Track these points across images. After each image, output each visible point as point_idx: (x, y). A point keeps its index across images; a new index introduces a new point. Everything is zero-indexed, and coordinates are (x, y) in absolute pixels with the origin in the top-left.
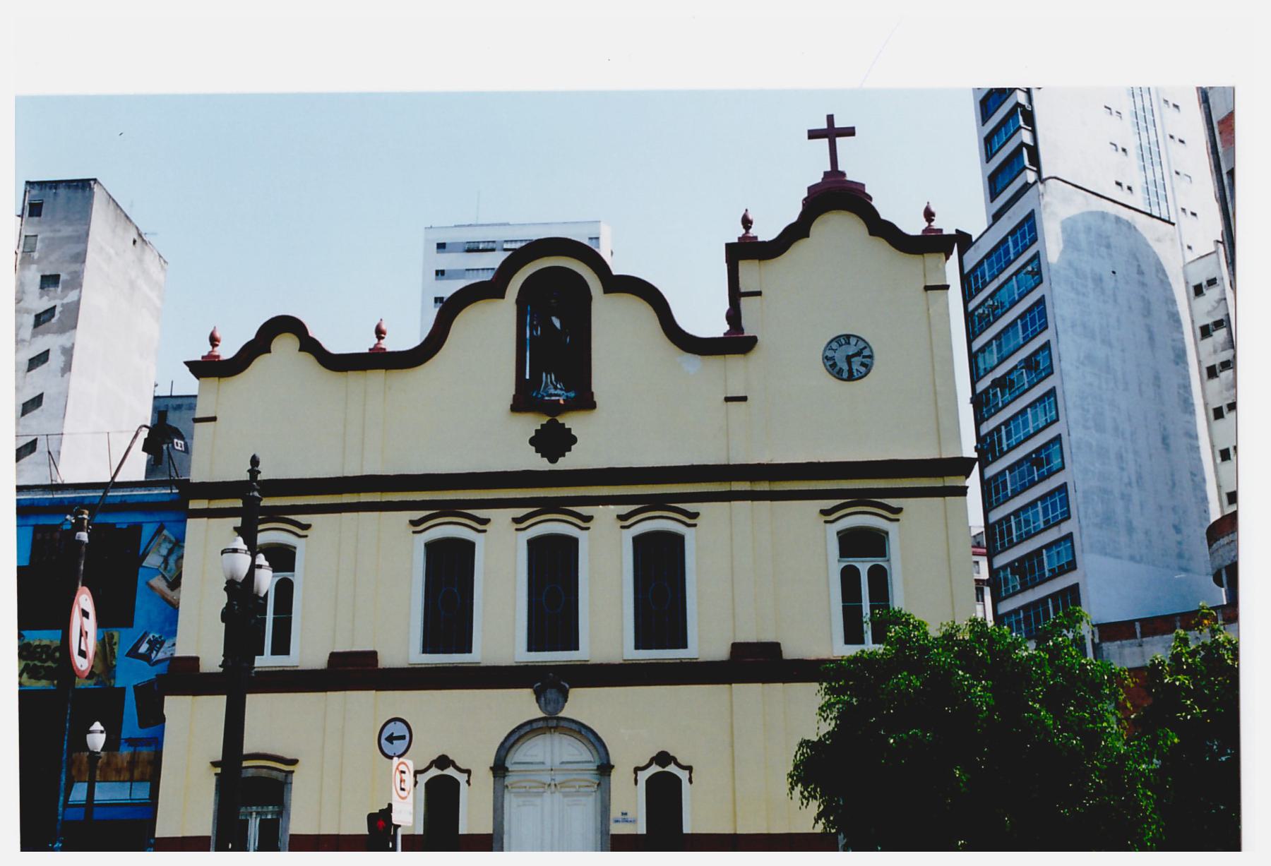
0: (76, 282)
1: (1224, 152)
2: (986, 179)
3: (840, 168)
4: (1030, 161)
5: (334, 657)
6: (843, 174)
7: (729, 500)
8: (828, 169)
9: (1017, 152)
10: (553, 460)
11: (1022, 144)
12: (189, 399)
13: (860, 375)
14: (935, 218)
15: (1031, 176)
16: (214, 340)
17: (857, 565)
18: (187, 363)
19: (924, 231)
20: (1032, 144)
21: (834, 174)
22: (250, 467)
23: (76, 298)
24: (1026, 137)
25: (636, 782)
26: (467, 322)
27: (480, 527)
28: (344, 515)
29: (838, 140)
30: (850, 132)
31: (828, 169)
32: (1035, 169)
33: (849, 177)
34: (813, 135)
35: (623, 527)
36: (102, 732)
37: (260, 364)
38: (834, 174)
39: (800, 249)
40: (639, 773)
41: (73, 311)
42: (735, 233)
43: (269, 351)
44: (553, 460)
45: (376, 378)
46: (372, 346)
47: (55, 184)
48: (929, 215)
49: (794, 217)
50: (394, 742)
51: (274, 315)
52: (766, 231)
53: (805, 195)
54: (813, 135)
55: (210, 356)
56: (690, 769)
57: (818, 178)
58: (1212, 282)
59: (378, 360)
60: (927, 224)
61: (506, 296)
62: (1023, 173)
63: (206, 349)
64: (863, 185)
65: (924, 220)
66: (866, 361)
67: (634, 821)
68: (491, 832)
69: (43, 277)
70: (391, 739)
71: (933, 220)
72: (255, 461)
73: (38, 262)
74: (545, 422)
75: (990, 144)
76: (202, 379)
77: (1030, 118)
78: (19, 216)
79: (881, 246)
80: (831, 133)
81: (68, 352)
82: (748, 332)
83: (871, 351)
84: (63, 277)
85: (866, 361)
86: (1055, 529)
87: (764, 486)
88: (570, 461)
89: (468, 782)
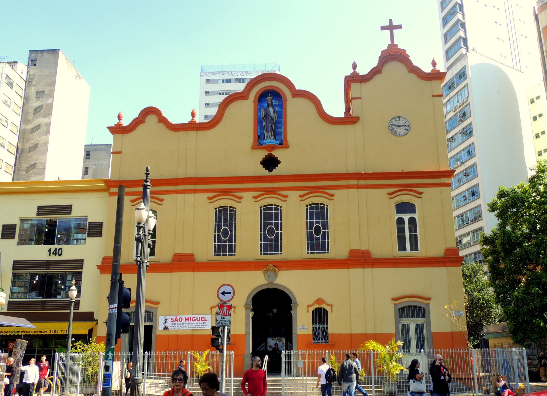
0: (51, 95)
1: (544, 42)
2: (445, 52)
3: (395, 43)
4: (463, 45)
5: (351, 252)
6: (396, 46)
7: (348, 188)
8: (390, 43)
9: (458, 40)
10: (270, 171)
11: (461, 37)
12: (96, 146)
13: (405, 134)
14: (437, 65)
15: (464, 51)
16: (119, 117)
18: (107, 127)
19: (432, 71)
20: (464, 37)
21: (392, 46)
23: (51, 102)
24: (462, 35)
25: (308, 311)
26: (234, 108)
28: (350, 190)
29: (394, 31)
30: (399, 27)
31: (390, 43)
32: (466, 48)
33: (399, 47)
34: (383, 28)
35: (301, 200)
36: (75, 290)
37: (141, 128)
38: (392, 46)
39: (378, 78)
41: (50, 107)
42: (349, 72)
44: (270, 171)
45: (192, 134)
46: (190, 121)
47: (42, 51)
48: (354, 66)
50: (225, 295)
51: (149, 106)
52: (363, 70)
53: (380, 55)
54: (383, 28)
55: (118, 124)
56: (331, 306)
57: (385, 48)
58: (538, 98)
59: (192, 126)
60: (433, 68)
61: (249, 98)
62: (461, 49)
63: (116, 121)
64: (405, 51)
65: (432, 66)
66: (407, 128)
68: (244, 332)
70: (223, 293)
71: (436, 66)
73: (35, 86)
75: (446, 37)
76: (115, 135)
77: (463, 25)
78: (27, 65)
79: (413, 76)
80: (391, 27)
81: (48, 125)
82: (354, 115)
83: (409, 123)
84: (46, 92)
85: (407, 128)
86: (473, 203)
87: (362, 182)
89: (332, 310)
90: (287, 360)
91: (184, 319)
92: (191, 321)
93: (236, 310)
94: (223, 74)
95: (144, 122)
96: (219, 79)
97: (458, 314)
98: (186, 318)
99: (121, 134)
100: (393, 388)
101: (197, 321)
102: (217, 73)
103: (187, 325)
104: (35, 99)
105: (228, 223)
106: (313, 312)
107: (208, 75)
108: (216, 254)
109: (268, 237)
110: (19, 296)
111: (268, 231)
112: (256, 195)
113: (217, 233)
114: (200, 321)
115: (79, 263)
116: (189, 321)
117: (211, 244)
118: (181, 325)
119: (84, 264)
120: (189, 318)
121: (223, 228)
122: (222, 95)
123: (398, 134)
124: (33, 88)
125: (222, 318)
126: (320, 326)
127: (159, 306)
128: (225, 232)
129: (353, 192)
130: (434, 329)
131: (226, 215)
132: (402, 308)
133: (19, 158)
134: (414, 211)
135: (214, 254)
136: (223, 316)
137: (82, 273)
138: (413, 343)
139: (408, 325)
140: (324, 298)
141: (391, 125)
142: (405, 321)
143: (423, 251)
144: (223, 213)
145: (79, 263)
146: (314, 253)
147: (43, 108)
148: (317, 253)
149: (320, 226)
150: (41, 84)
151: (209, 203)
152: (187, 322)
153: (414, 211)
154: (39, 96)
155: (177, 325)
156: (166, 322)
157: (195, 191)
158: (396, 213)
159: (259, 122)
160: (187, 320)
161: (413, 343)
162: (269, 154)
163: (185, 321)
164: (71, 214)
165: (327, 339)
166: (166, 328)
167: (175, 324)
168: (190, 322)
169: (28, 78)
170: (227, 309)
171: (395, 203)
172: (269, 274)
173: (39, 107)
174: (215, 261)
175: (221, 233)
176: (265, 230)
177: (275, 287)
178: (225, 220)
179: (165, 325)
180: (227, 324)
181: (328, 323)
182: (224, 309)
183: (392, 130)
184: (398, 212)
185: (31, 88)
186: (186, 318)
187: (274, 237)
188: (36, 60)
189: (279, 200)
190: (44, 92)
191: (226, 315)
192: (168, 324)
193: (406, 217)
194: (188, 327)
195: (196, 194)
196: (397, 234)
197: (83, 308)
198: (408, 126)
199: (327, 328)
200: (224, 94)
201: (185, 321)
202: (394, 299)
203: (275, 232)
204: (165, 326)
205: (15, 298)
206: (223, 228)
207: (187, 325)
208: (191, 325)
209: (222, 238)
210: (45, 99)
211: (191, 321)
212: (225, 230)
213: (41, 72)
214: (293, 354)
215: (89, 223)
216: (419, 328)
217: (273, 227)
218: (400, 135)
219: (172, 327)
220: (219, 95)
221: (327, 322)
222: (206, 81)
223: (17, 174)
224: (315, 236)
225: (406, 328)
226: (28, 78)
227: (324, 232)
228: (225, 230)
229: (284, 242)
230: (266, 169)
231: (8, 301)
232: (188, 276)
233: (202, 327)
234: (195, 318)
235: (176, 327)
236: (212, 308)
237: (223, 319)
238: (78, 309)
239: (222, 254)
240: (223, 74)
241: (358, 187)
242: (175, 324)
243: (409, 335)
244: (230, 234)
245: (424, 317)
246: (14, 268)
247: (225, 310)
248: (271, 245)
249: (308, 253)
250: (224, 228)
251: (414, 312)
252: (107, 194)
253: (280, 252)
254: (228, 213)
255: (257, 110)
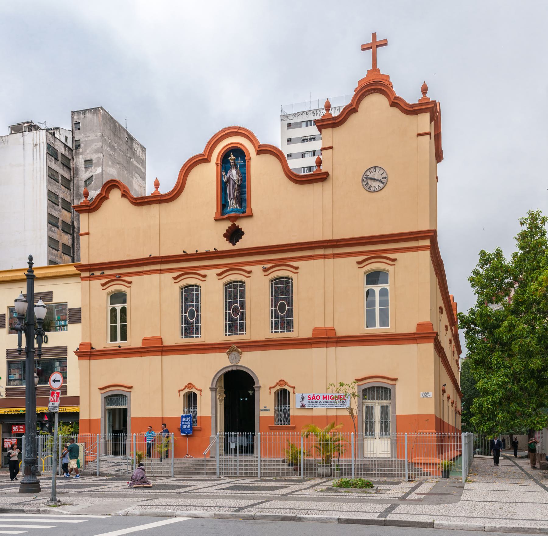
10: (234, 244)
13: (380, 189)
17: (373, 288)
22: (28, 261)
25: (180, 395)
27: (203, 279)
28: (316, 261)
30: (384, 43)
34: (365, 48)
39: (354, 119)
40: (180, 392)
43: (441, 162)
44: (234, 244)
45: (154, 209)
47: (84, 111)
48: (424, 90)
49: (348, 102)
54: (365, 48)
56: (294, 388)
67: (269, 410)
68: (210, 415)
69: (85, 161)
72: (31, 258)
74: (230, 226)
79: (396, 111)
83: (387, 174)
84: (94, 161)
87: (330, 251)
88: (243, 244)
89: (201, 394)
90: (226, 442)
91: (321, 397)
92: (329, 399)
93: (295, 390)
94: (307, 114)
95: (108, 198)
96: (302, 122)
97: (425, 396)
98: (323, 396)
99: (87, 214)
100: (327, 471)
101: (317, 399)
102: (300, 114)
103: (325, 403)
104: (84, 169)
105: (194, 303)
106: (275, 393)
107: (289, 118)
108: (184, 336)
109: (233, 316)
110: (16, 383)
111: (233, 310)
112: (360, 260)
113: (184, 315)
114: (339, 400)
115: (64, 349)
116: (327, 399)
117: (221, 322)
118: (319, 403)
119: (68, 351)
120: (327, 396)
121: (279, 303)
122: (306, 142)
123: (372, 189)
124: (81, 156)
125: (53, 404)
126: (279, 408)
127: (132, 390)
128: (192, 312)
129: (319, 262)
130: (399, 412)
131: (236, 292)
132: (366, 389)
133: (77, 237)
134: (125, 302)
135: (181, 336)
136: (54, 403)
137: (66, 359)
138: (377, 427)
139: (372, 407)
140: (194, 384)
141: (365, 179)
142: (369, 403)
143: (388, 329)
144: (189, 293)
145: (64, 349)
146: (278, 332)
147: (93, 179)
148: (281, 332)
149: (285, 302)
150: (88, 151)
151: (175, 283)
152: (325, 400)
153: (125, 302)
154: (87, 166)
155: (314, 403)
156: (303, 399)
157: (161, 271)
158: (367, 284)
159: (223, 186)
160: (325, 398)
161: (377, 427)
162: (232, 225)
163: (323, 399)
164: (52, 301)
165: (289, 421)
166: (303, 406)
167: (312, 402)
168: (328, 400)
169: (74, 145)
170: (57, 396)
171: (365, 273)
172: (233, 356)
173: (89, 179)
174: (268, 339)
175: (187, 314)
176: (230, 309)
177: (239, 368)
178: (236, 297)
179: (302, 403)
180: (57, 409)
181: (289, 405)
182: (54, 396)
183: (365, 185)
184: (368, 283)
185: (79, 157)
186: (323, 396)
187: (238, 316)
188: (79, 123)
189: (387, 265)
190: (92, 160)
191: (56, 402)
192: (305, 402)
193: (119, 307)
194: (326, 406)
195: (335, 259)
196: (366, 308)
197: (71, 393)
198: (385, 178)
199: (289, 410)
200: (309, 140)
201: (323, 399)
202: (101, 389)
203: (240, 311)
204: (302, 404)
205: (11, 385)
206: (279, 303)
207: (325, 403)
208: (329, 403)
209: (189, 320)
210: (94, 168)
211: (329, 399)
212: (192, 310)
213: (86, 137)
214: (93, 437)
215: (69, 309)
216: (385, 411)
217: (238, 305)
218: (375, 190)
219: (310, 406)
220: (303, 142)
221: (289, 404)
222: (287, 126)
223: (77, 255)
224: (280, 313)
225: (370, 411)
226: (74, 145)
227: (289, 310)
228: (192, 310)
229: (202, 324)
230: (229, 243)
231: (6, 388)
232: (156, 359)
233: (341, 406)
234: (333, 396)
235: (313, 406)
236: (180, 391)
237: (53, 406)
238: (66, 395)
239: (279, 330)
240: (307, 114)
241: (325, 257)
242: (312, 402)
243: (372, 418)
244: (197, 315)
245: (390, 399)
246: (7, 357)
247: (55, 397)
248: (236, 325)
249: (272, 332)
250: (190, 309)
251: (119, 400)
252: (78, 280)
253: (291, 330)
254: (285, 285)
255: (220, 177)
